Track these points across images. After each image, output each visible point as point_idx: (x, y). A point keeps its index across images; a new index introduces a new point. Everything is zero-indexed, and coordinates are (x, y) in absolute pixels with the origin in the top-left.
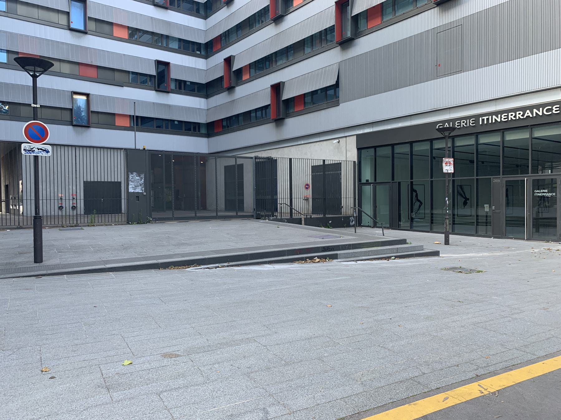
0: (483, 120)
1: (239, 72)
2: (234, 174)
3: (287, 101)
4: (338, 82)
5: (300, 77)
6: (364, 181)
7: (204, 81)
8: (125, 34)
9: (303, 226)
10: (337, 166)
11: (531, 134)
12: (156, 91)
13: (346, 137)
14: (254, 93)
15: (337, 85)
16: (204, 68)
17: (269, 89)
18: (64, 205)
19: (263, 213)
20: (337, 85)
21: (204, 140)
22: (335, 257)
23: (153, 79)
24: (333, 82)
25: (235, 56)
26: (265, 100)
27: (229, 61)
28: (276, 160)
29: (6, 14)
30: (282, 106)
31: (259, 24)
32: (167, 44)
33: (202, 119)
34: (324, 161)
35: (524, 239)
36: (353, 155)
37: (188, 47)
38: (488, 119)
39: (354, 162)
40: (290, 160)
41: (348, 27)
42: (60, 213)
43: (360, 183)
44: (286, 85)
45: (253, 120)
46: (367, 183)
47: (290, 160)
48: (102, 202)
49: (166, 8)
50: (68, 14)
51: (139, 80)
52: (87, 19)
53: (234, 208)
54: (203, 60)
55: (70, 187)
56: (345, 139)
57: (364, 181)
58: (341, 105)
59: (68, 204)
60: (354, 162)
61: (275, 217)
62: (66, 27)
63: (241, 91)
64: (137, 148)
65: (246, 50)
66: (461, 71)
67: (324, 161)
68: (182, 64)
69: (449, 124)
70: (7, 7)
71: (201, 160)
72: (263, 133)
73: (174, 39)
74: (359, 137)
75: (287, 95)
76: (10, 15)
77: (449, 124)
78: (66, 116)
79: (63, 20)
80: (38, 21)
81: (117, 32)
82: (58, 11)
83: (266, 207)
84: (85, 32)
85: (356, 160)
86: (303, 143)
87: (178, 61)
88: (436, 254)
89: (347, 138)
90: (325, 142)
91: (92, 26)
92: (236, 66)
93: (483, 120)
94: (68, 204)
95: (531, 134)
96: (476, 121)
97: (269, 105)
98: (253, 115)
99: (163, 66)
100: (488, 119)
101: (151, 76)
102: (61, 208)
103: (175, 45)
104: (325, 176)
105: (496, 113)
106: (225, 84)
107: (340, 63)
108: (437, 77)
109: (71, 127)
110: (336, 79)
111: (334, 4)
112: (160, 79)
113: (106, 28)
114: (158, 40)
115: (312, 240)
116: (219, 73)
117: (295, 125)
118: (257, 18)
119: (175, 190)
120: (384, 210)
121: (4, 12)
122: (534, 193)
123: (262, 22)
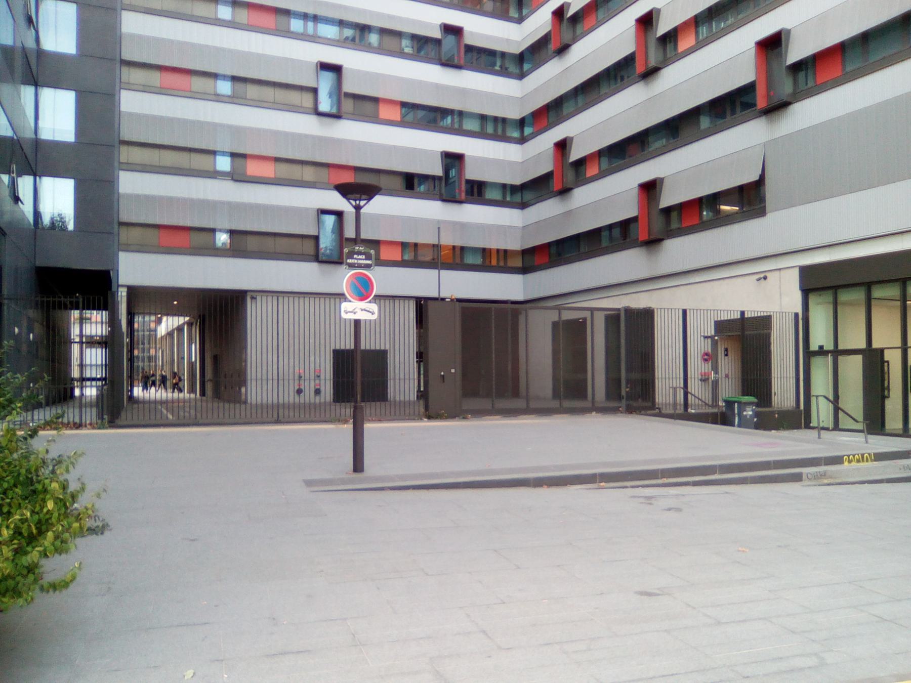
1: (580, 164)
2: (572, 333)
3: (668, 211)
5: (686, 170)
6: (814, 347)
7: (518, 182)
9: (736, 429)
10: (765, 322)
12: (444, 200)
13: (780, 269)
14: (610, 197)
15: (760, 183)
16: (519, 159)
17: (636, 190)
18: (322, 389)
19: (635, 404)
20: (760, 183)
21: (517, 279)
22: (797, 478)
23: (437, 182)
24: (754, 177)
27: (562, 146)
28: (653, 311)
29: (230, 100)
30: (659, 221)
32: (504, 131)
33: (515, 245)
34: (743, 313)
36: (793, 301)
37: (495, 127)
39: (796, 315)
40: (685, 312)
42: (297, 400)
43: (808, 356)
44: (666, 184)
45: (605, 243)
46: (821, 352)
47: (685, 312)
48: (357, 380)
49: (458, 67)
50: (315, 91)
52: (338, 93)
53: (571, 394)
54: (518, 146)
55: (312, 358)
56: (777, 273)
57: (814, 347)
59: (309, 388)
60: (796, 315)
61: (657, 411)
62: (312, 111)
63: (583, 195)
64: (437, 271)
65: (591, 128)
67: (743, 313)
68: (486, 156)
70: (233, 90)
71: (509, 313)
73: (472, 115)
74: (806, 272)
75: (667, 199)
76: (236, 100)
78: (309, 247)
79: (306, 100)
80: (275, 106)
82: (301, 88)
83: (634, 389)
84: (337, 116)
85: (799, 309)
86: (697, 280)
88: (819, 282)
90: (740, 280)
91: (348, 105)
92: (575, 154)
94: (309, 388)
97: (634, 220)
98: (605, 234)
99: (453, 160)
101: (434, 178)
102: (299, 392)
103: (471, 125)
104: (746, 339)
106: (556, 185)
107: (765, 144)
109: (314, 266)
110: (760, 172)
111: (753, 45)
112: (452, 182)
113: (368, 106)
114: (433, 117)
115: (758, 450)
117: (681, 251)
118: (613, 73)
119: (476, 361)
120: (854, 399)
121: (229, 96)
123: (622, 79)
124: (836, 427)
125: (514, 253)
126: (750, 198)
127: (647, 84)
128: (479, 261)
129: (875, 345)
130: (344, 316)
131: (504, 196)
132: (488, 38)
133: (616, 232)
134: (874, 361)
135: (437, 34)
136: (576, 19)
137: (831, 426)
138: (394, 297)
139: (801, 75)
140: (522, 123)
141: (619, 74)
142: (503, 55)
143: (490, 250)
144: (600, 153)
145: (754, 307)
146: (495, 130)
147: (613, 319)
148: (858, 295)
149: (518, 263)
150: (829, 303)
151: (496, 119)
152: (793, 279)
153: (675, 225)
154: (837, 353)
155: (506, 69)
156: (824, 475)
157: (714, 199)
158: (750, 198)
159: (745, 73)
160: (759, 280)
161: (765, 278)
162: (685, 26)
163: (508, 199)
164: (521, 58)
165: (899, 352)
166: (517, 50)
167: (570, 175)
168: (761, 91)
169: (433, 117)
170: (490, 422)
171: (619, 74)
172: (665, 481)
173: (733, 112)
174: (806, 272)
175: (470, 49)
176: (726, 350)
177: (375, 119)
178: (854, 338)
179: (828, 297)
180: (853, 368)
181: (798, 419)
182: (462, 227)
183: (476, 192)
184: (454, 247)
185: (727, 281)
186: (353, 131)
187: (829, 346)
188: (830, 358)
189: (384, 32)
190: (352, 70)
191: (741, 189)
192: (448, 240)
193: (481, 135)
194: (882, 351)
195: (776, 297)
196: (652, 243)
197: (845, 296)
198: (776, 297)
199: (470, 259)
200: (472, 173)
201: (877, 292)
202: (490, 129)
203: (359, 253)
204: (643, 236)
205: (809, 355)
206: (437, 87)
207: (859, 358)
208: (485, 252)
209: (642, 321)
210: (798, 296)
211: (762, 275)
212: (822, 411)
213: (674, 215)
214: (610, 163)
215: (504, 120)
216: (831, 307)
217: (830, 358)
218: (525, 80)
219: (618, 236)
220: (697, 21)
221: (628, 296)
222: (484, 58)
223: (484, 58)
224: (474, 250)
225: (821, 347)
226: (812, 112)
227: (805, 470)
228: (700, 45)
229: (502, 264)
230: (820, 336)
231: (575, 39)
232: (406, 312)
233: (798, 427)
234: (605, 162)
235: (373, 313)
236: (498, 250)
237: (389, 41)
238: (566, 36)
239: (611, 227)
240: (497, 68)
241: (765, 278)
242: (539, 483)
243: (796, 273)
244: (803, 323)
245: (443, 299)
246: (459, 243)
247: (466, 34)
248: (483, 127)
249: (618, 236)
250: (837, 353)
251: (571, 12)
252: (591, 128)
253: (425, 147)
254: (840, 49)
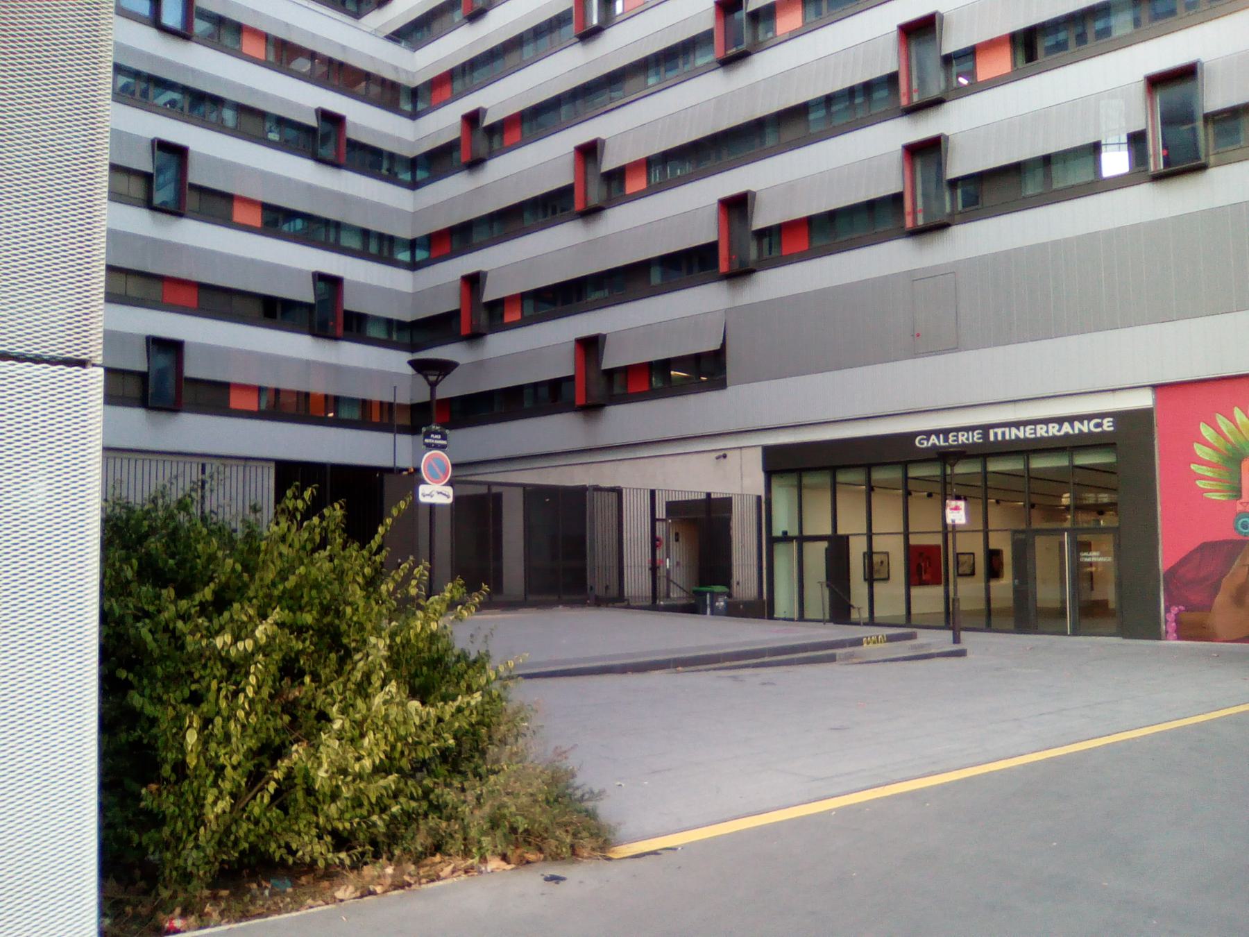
0: (996, 434)
3: (610, 373)
4: (724, 345)
7: (407, 317)
8: (255, 218)
10: (726, 503)
11: (1071, 461)
22: (832, 659)
24: (714, 345)
25: (605, 336)
26: (563, 367)
28: (730, 499)
30: (598, 383)
31: (545, 216)
32: (391, 251)
35: (1065, 634)
37: (379, 246)
38: (1003, 434)
39: (759, 498)
41: (739, 25)
43: (770, 541)
45: (527, 404)
46: (786, 538)
47: (653, 493)
51: (273, 311)
56: (738, 452)
58: (729, 388)
60: (759, 498)
63: (499, 344)
64: (391, 436)
65: (514, 263)
66: (956, 349)
68: (371, 283)
69: (946, 440)
72: (558, 430)
74: (770, 454)
75: (611, 360)
77: (946, 440)
81: (240, 213)
87: (357, 272)
88: (784, 463)
89: (744, 451)
93: (996, 434)
95: (1071, 461)
96: (985, 435)
99: (330, 284)
100: (1003, 434)
104: (704, 523)
105: (1017, 424)
107: (726, 311)
108: (915, 355)
114: (316, 229)
116: (450, 303)
117: (625, 420)
122: (1079, 557)
123: (554, 212)
124: (802, 618)
125: (402, 407)
126: (708, 370)
127: (587, 222)
128: (355, 414)
129: (841, 531)
130: (422, 499)
131: (389, 333)
132: (373, 132)
133: (544, 392)
134: (838, 547)
135: (312, 121)
136: (493, 130)
137: (796, 616)
138: (247, 459)
139: (766, 241)
140: (413, 245)
141: (550, 207)
142: (392, 156)
143: (371, 402)
144: (523, 296)
145: (719, 489)
146: (380, 250)
147: (534, 494)
148: (823, 479)
149: (405, 420)
150: (792, 486)
151: (381, 237)
152: (756, 458)
153: (617, 390)
154: (802, 539)
155: (396, 174)
156: (851, 656)
157: (665, 365)
158: (708, 370)
159: (705, 231)
160: (718, 458)
161: (725, 456)
162: (635, 165)
163: (395, 337)
164: (413, 164)
165: (864, 539)
166: (410, 153)
167: (483, 317)
168: (723, 252)
169: (316, 229)
170: (489, 616)
171: (550, 207)
172: (728, 664)
173: (690, 271)
174: (770, 454)
175: (355, 145)
176: (677, 534)
177: (227, 221)
178: (819, 524)
179: (792, 480)
180: (816, 554)
181: (762, 608)
182: (337, 370)
183: (354, 327)
184: (326, 397)
185: (680, 457)
186: (195, 234)
187: (794, 532)
188: (795, 544)
189: (241, 109)
190: (199, 154)
191: (698, 357)
192: (318, 386)
193: (363, 254)
194: (846, 538)
195: (739, 478)
196: (591, 408)
197: (808, 480)
198: (739, 478)
199: (345, 414)
200: (351, 302)
201: (841, 477)
202: (373, 248)
203: (436, 433)
204: (580, 400)
205: (772, 541)
206: (310, 188)
207: (825, 544)
208: (365, 404)
209: (573, 502)
210: (760, 477)
211: (721, 453)
212: (784, 600)
213: (618, 378)
214: (536, 309)
215: (391, 239)
216: (795, 492)
217: (795, 544)
218: (419, 191)
219: (548, 397)
220: (649, 164)
221: (559, 469)
222: (371, 160)
223: (371, 160)
224: (352, 401)
225: (785, 533)
226: (779, 283)
227: (838, 652)
228: (651, 190)
229: (386, 420)
230: (783, 522)
231: (492, 154)
232: (259, 479)
233: (762, 617)
234: (529, 309)
235: (448, 497)
236: (381, 403)
237: (250, 123)
238: (482, 147)
239: (536, 385)
240: (384, 171)
241: (725, 456)
242: (623, 669)
243: (759, 452)
244: (765, 506)
245: (402, 470)
246: (332, 391)
247: (348, 125)
248: (366, 244)
249: (548, 397)
250: (802, 539)
251: (488, 121)
252: (514, 263)
253: (293, 264)
254: (809, 223)
